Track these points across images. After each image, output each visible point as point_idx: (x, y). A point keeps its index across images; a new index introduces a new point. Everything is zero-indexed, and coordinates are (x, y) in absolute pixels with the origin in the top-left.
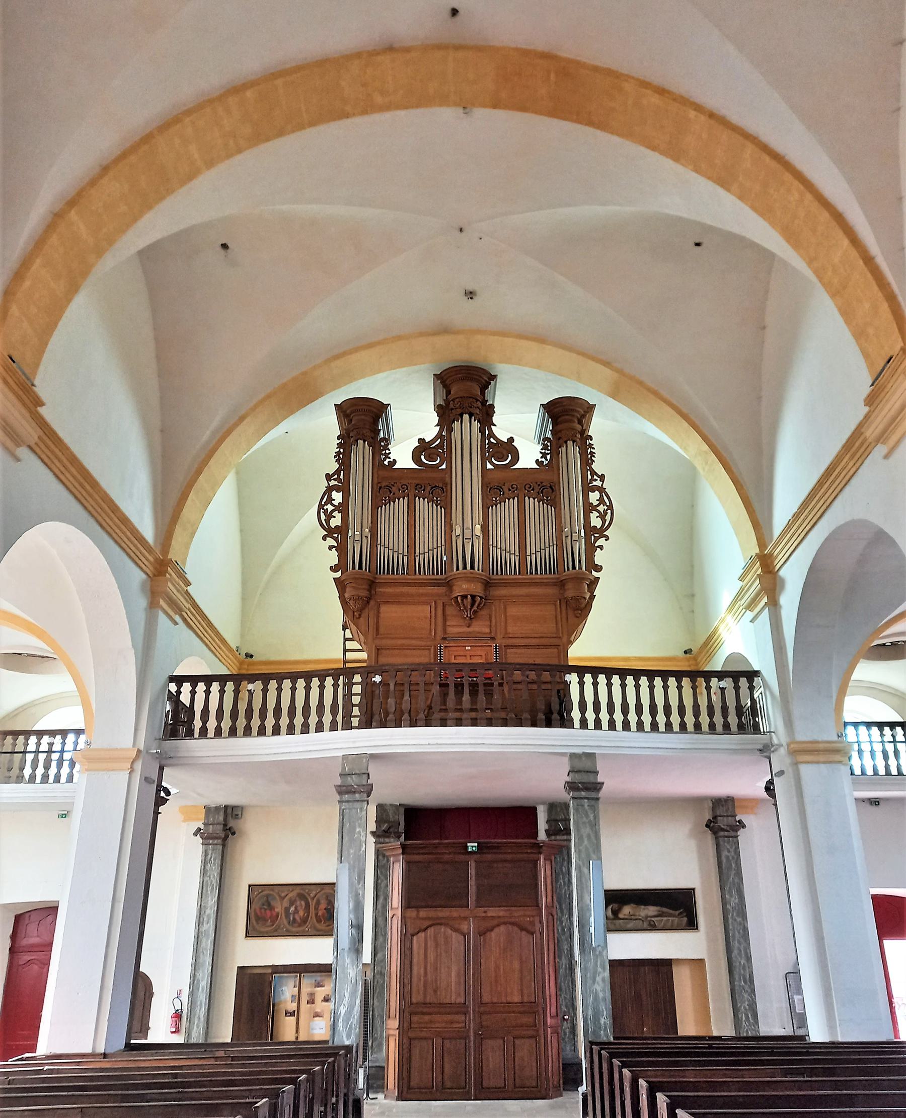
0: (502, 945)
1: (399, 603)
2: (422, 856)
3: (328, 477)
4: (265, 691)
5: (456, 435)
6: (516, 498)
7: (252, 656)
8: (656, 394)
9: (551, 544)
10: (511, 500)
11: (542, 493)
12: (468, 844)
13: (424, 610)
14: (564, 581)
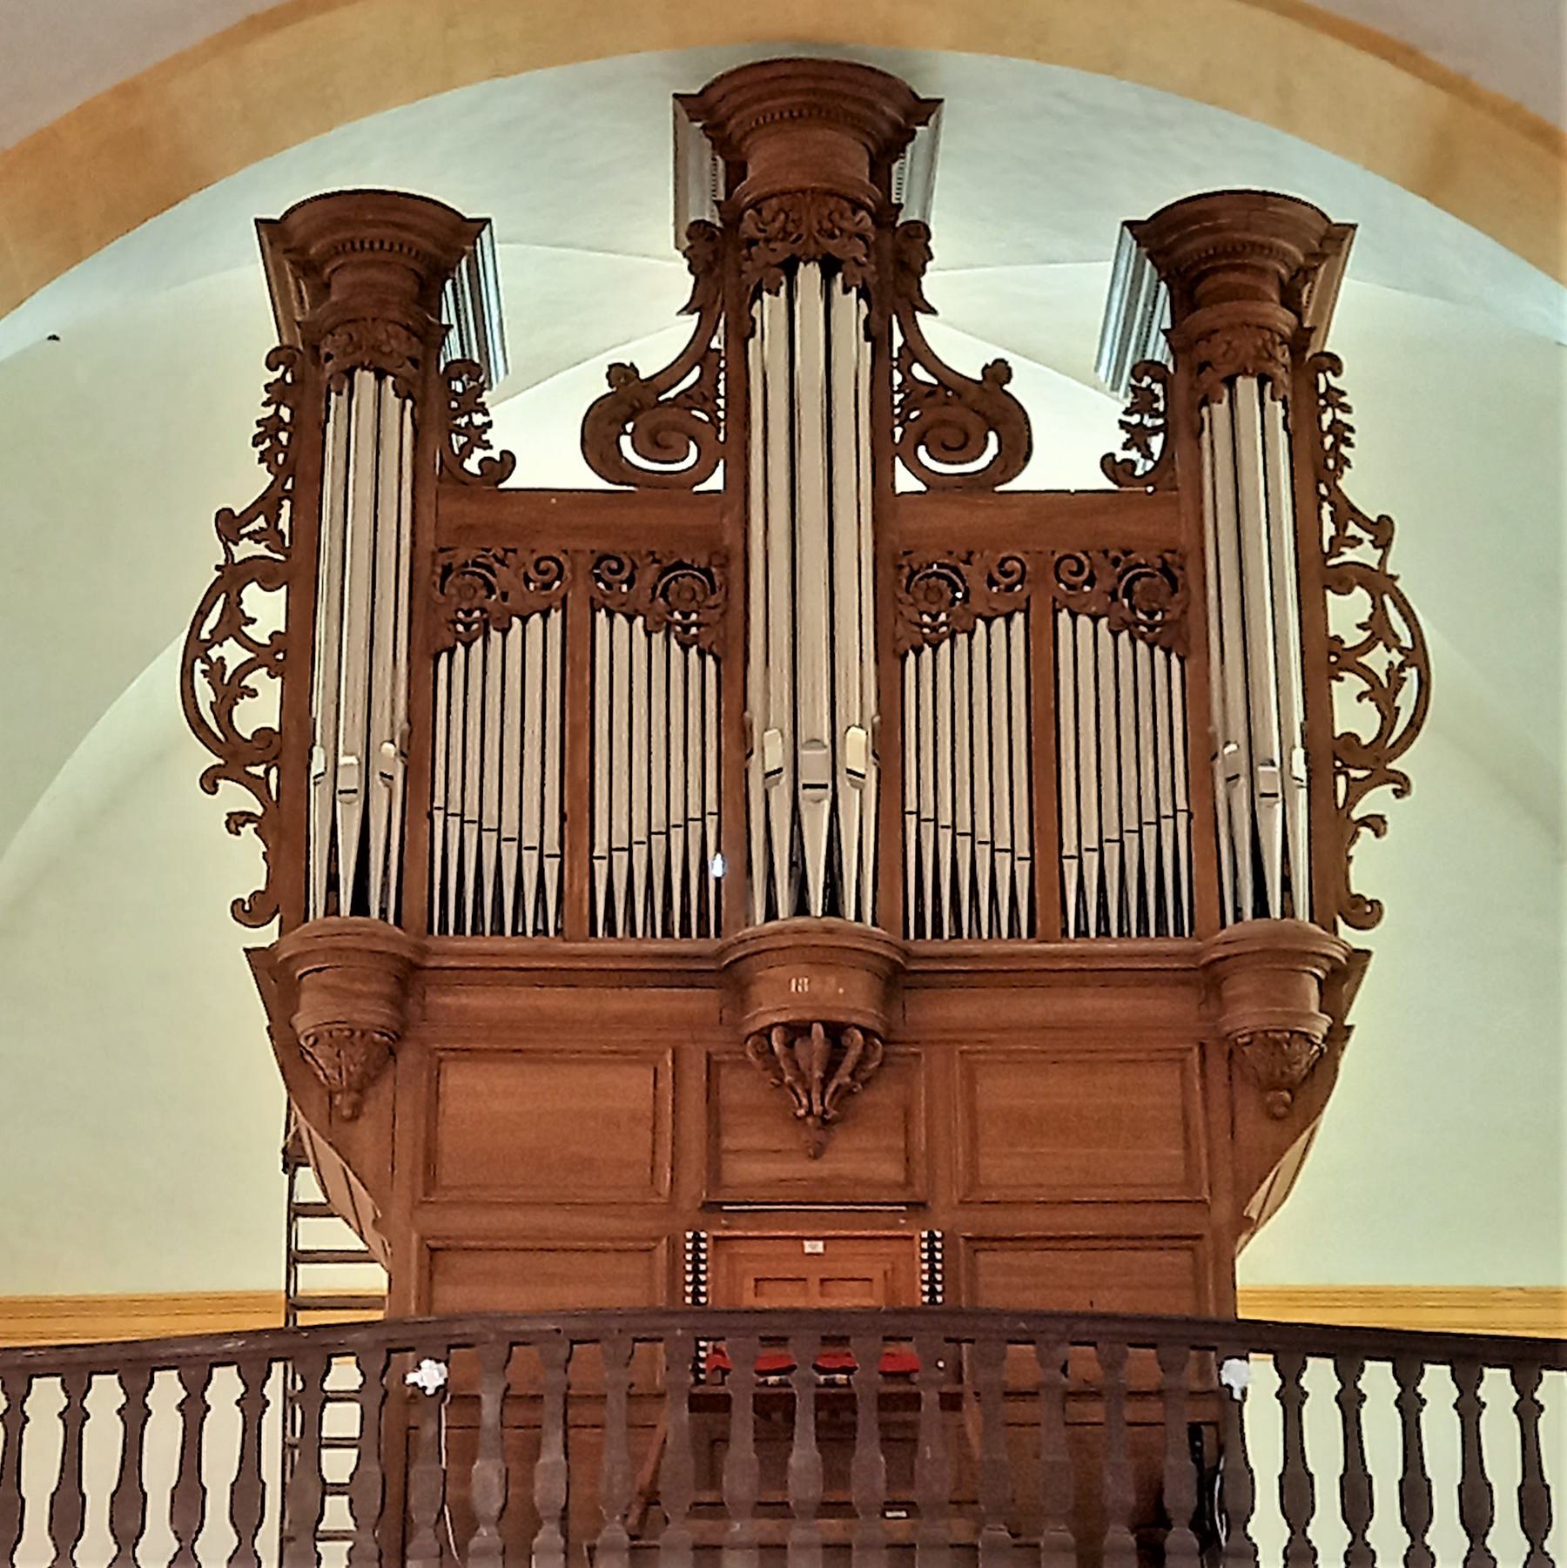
3: (229, 525)
5: (765, 352)
6: (1019, 618)
9: (1166, 810)
11: (1128, 593)
14: (1219, 967)
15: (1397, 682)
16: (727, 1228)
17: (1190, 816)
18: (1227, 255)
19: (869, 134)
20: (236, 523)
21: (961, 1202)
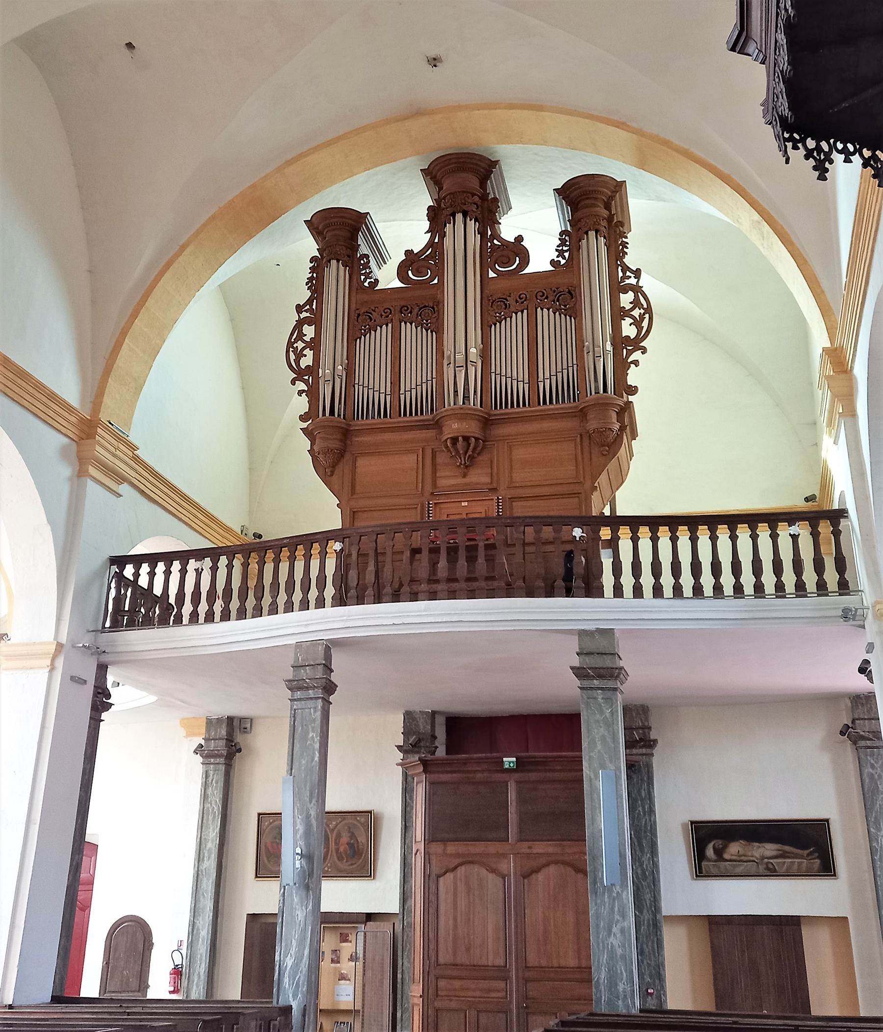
0: (551, 893)
1: (380, 453)
2: (449, 775)
3: (299, 309)
4: (214, 569)
5: (448, 242)
6: (525, 311)
7: (260, 536)
8: (687, 154)
9: (570, 365)
10: (519, 313)
11: (558, 300)
12: (505, 759)
13: (410, 460)
14: (585, 410)
15: (642, 317)
16: (438, 500)
17: (577, 366)
18: (584, 195)
19: (477, 174)
20: (302, 308)
21: (507, 487)
